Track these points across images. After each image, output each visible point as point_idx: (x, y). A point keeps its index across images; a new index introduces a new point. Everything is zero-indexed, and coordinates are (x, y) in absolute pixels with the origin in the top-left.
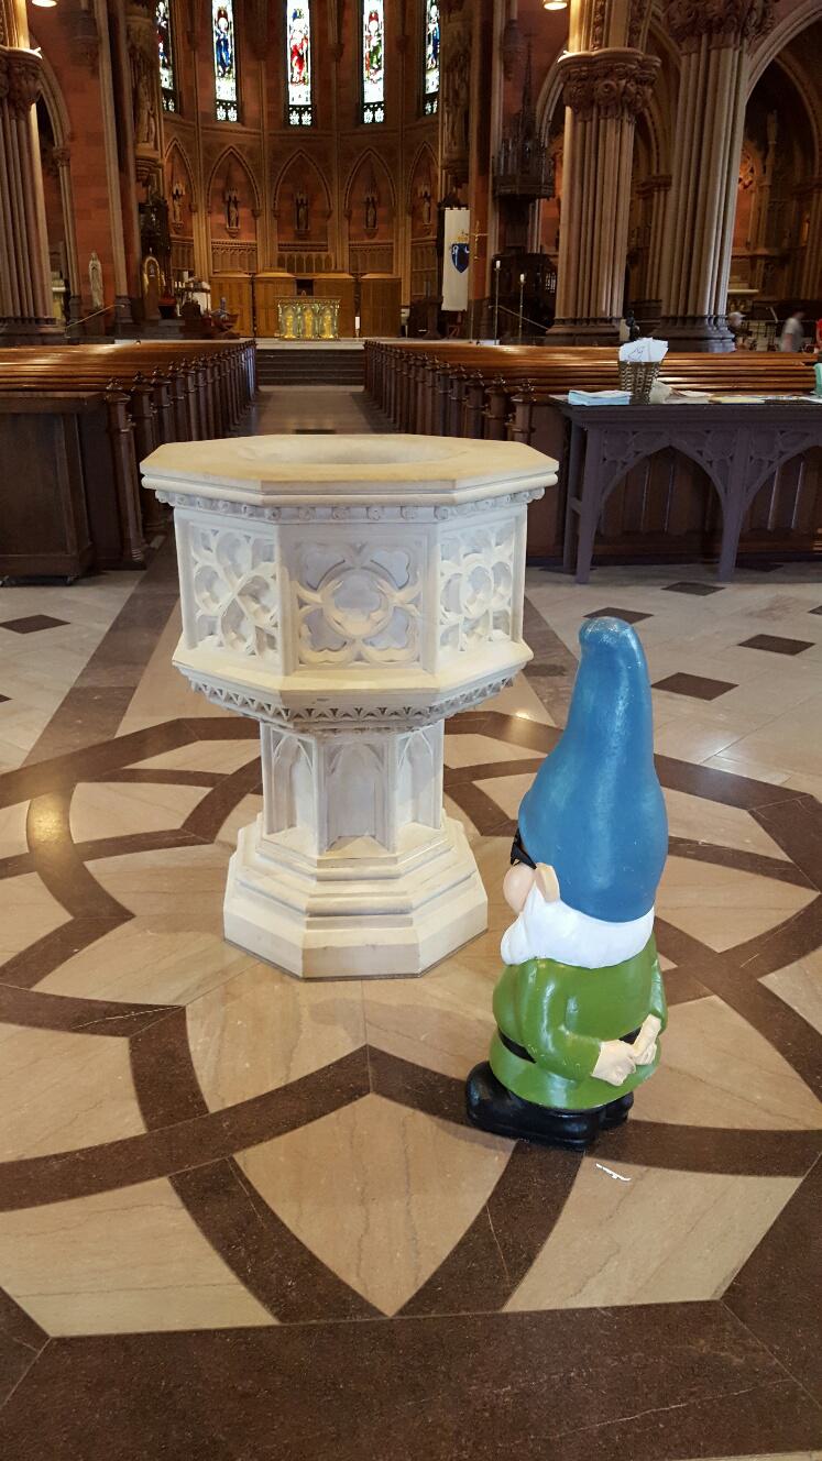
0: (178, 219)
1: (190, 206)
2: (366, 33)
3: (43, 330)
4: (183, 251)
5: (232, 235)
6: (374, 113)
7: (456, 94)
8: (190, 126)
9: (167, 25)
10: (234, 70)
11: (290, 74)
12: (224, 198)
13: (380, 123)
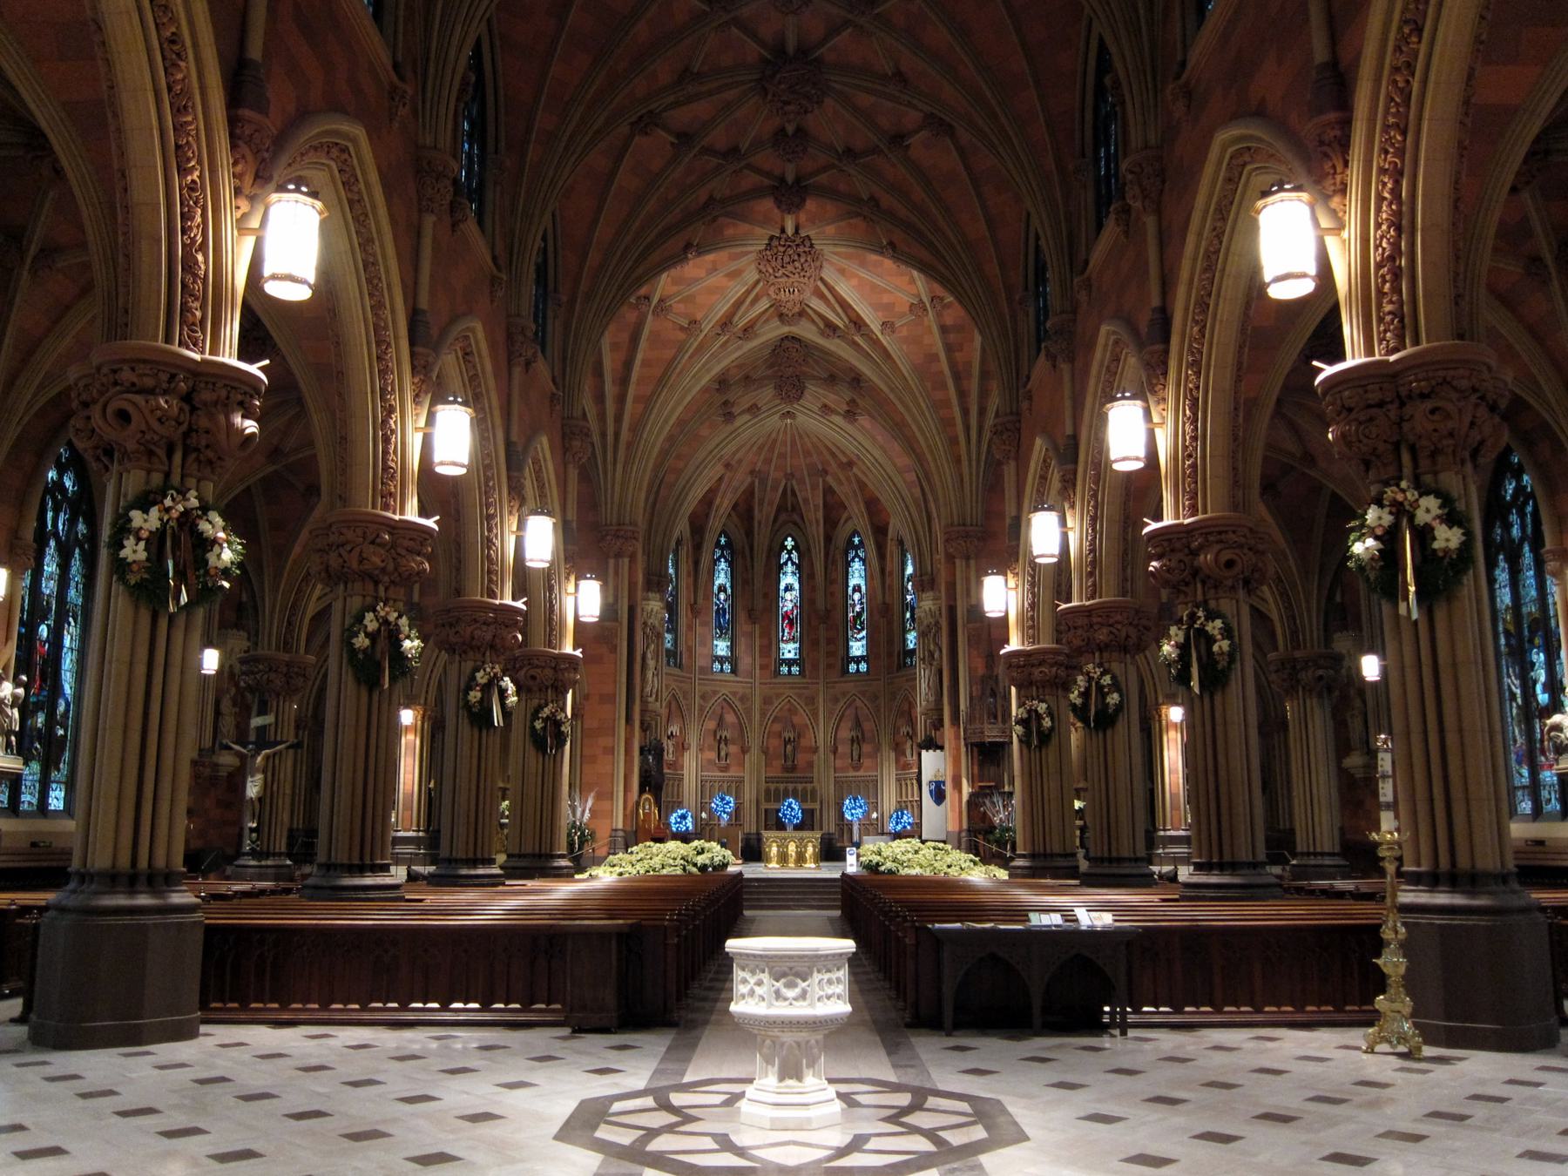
2: (850, 602)
3: (556, 864)
7: (932, 655)
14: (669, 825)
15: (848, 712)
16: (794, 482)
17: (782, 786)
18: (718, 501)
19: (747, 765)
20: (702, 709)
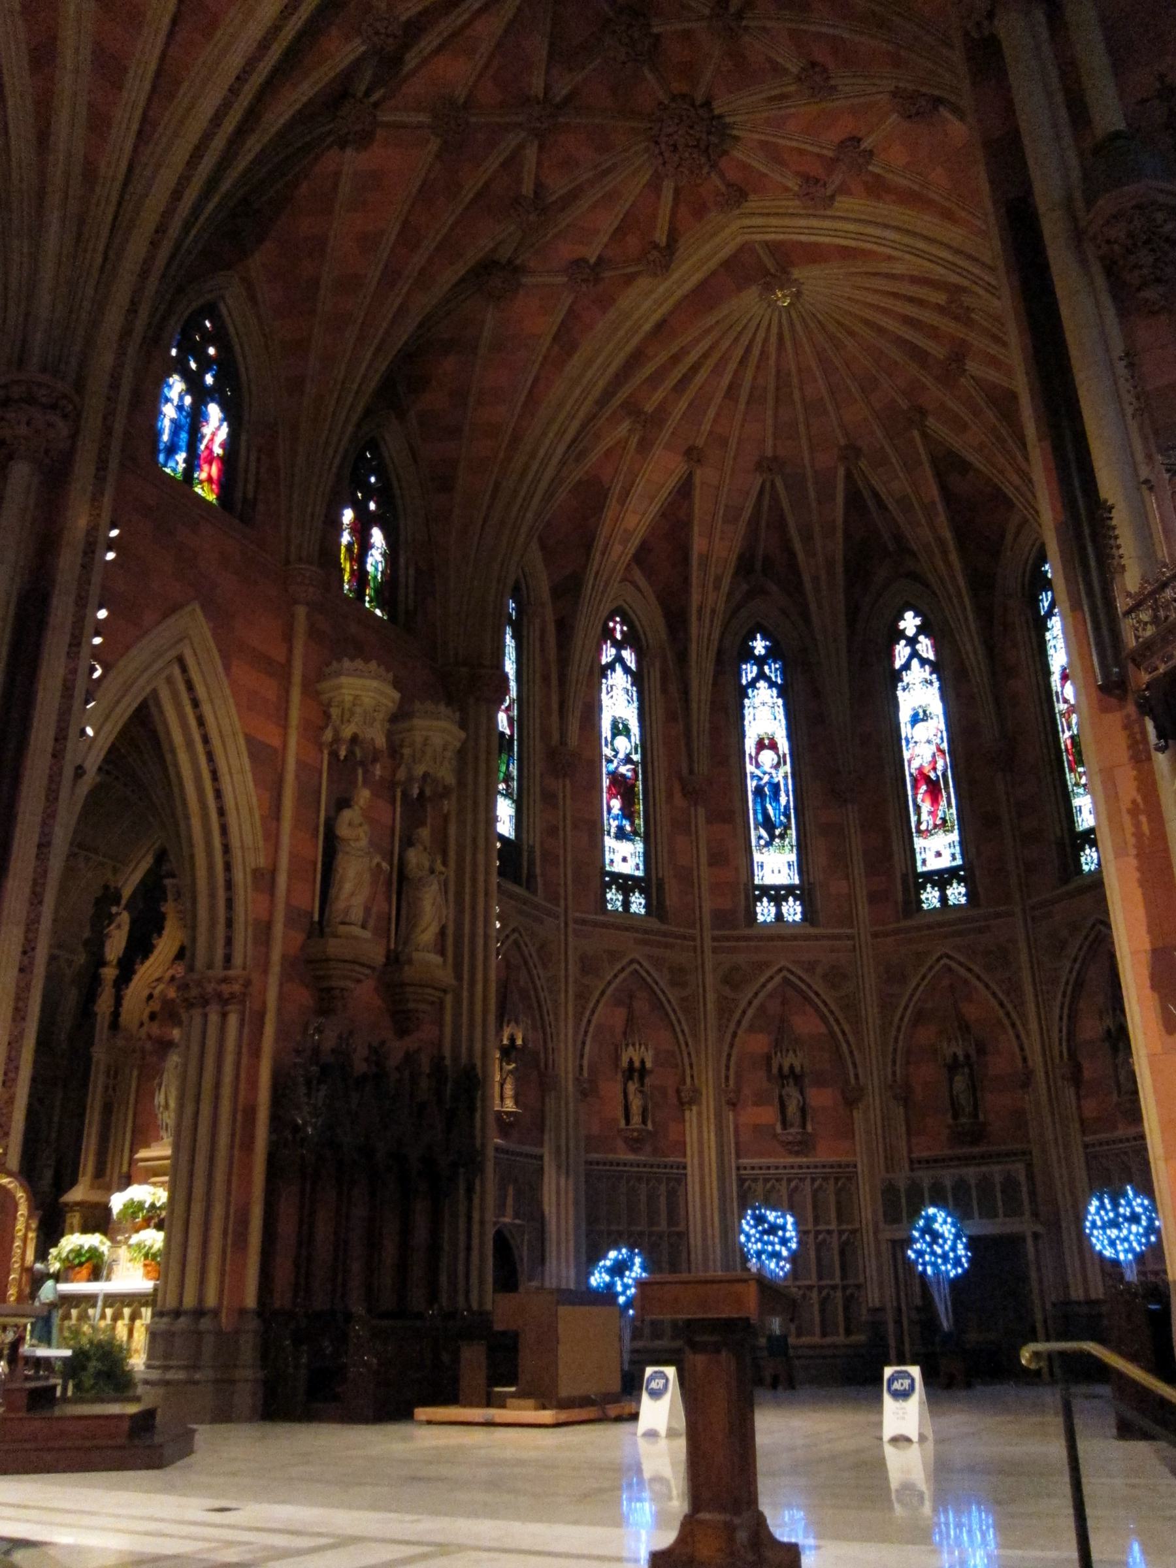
0: (636, 1119)
1: (678, 1091)
5: (804, 1145)
9: (635, 771)
10: (793, 832)
11: (913, 819)
12: (769, 1070)
20: (725, 1009)
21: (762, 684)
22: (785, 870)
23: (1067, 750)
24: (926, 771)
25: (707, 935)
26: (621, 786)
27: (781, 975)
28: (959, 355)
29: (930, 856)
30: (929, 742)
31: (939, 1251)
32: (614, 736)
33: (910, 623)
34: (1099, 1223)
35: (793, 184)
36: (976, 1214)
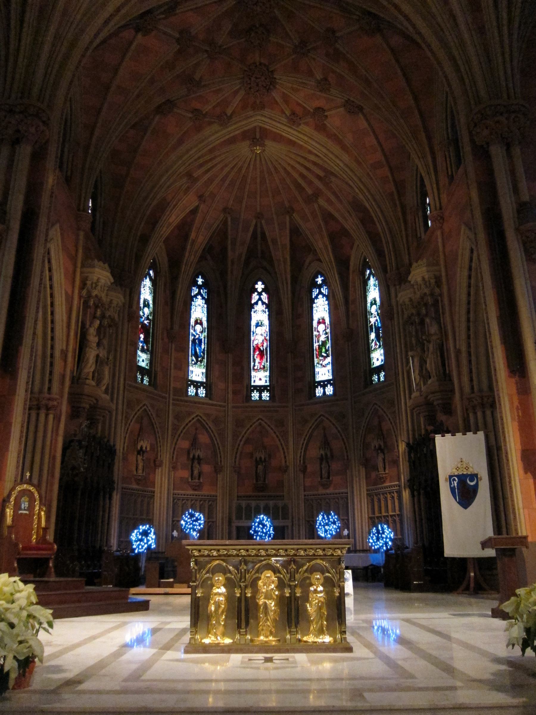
0: (140, 472)
1: (155, 461)
2: (315, 333)
4: (142, 501)
6: (324, 389)
8: (163, 397)
9: (149, 323)
11: (252, 364)
13: (330, 395)
14: (130, 543)
15: (315, 433)
16: (263, 222)
17: (253, 504)
18: (193, 235)
19: (220, 483)
20: (175, 428)
21: (199, 297)
22: (201, 375)
23: (316, 350)
24: (259, 346)
25: (230, 406)
26: (145, 329)
27: (197, 418)
28: (317, 194)
29: (257, 380)
30: (262, 335)
31: (264, 531)
32: (144, 307)
33: (260, 286)
34: (322, 524)
35: (288, 113)
36: (280, 518)
